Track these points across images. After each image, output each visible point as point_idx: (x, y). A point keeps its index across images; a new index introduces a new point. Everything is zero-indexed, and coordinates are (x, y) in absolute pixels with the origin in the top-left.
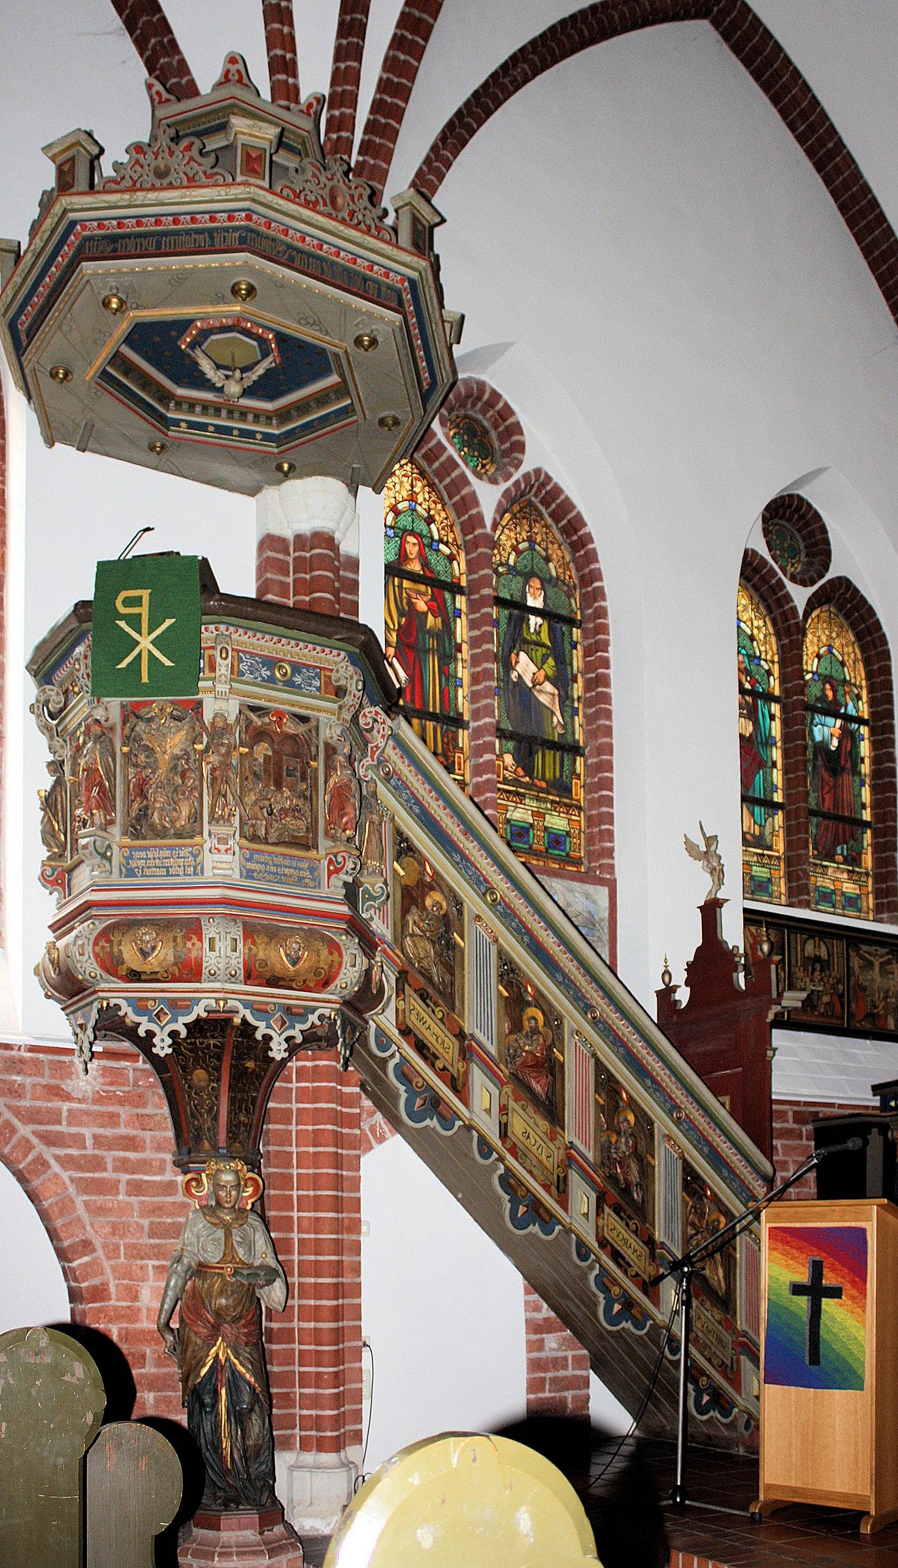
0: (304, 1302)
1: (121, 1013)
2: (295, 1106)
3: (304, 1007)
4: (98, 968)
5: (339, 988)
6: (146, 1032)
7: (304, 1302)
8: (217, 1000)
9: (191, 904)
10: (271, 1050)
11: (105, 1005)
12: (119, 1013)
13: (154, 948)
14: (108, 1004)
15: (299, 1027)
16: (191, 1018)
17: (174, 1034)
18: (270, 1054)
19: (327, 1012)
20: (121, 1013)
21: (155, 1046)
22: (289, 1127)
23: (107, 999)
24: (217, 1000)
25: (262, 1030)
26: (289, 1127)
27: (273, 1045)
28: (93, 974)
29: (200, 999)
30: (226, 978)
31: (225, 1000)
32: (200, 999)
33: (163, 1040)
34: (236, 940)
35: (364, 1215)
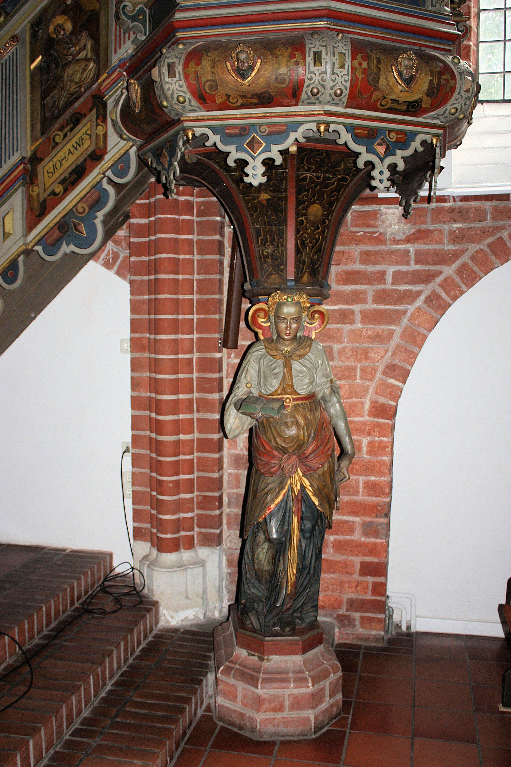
0: (188, 416)
1: (293, 149)
2: (194, 237)
3: (286, 124)
4: (188, 93)
5: (447, 112)
6: (235, 161)
7: (188, 416)
8: (319, 123)
9: (431, 36)
10: (247, 175)
11: (190, 135)
12: (207, 144)
13: (251, 68)
14: (193, 134)
15: (400, 153)
16: (409, 152)
17: (268, 163)
18: (247, 180)
19: (428, 138)
20: (293, 149)
21: (374, 179)
22: (199, 257)
23: (191, 128)
24: (319, 123)
25: (365, 157)
26: (199, 257)
27: (375, 173)
28: (181, 99)
29: (416, 134)
30: (329, 99)
31: (328, 124)
32: (416, 134)
33: (381, 173)
34: (344, 54)
35: (127, 357)
